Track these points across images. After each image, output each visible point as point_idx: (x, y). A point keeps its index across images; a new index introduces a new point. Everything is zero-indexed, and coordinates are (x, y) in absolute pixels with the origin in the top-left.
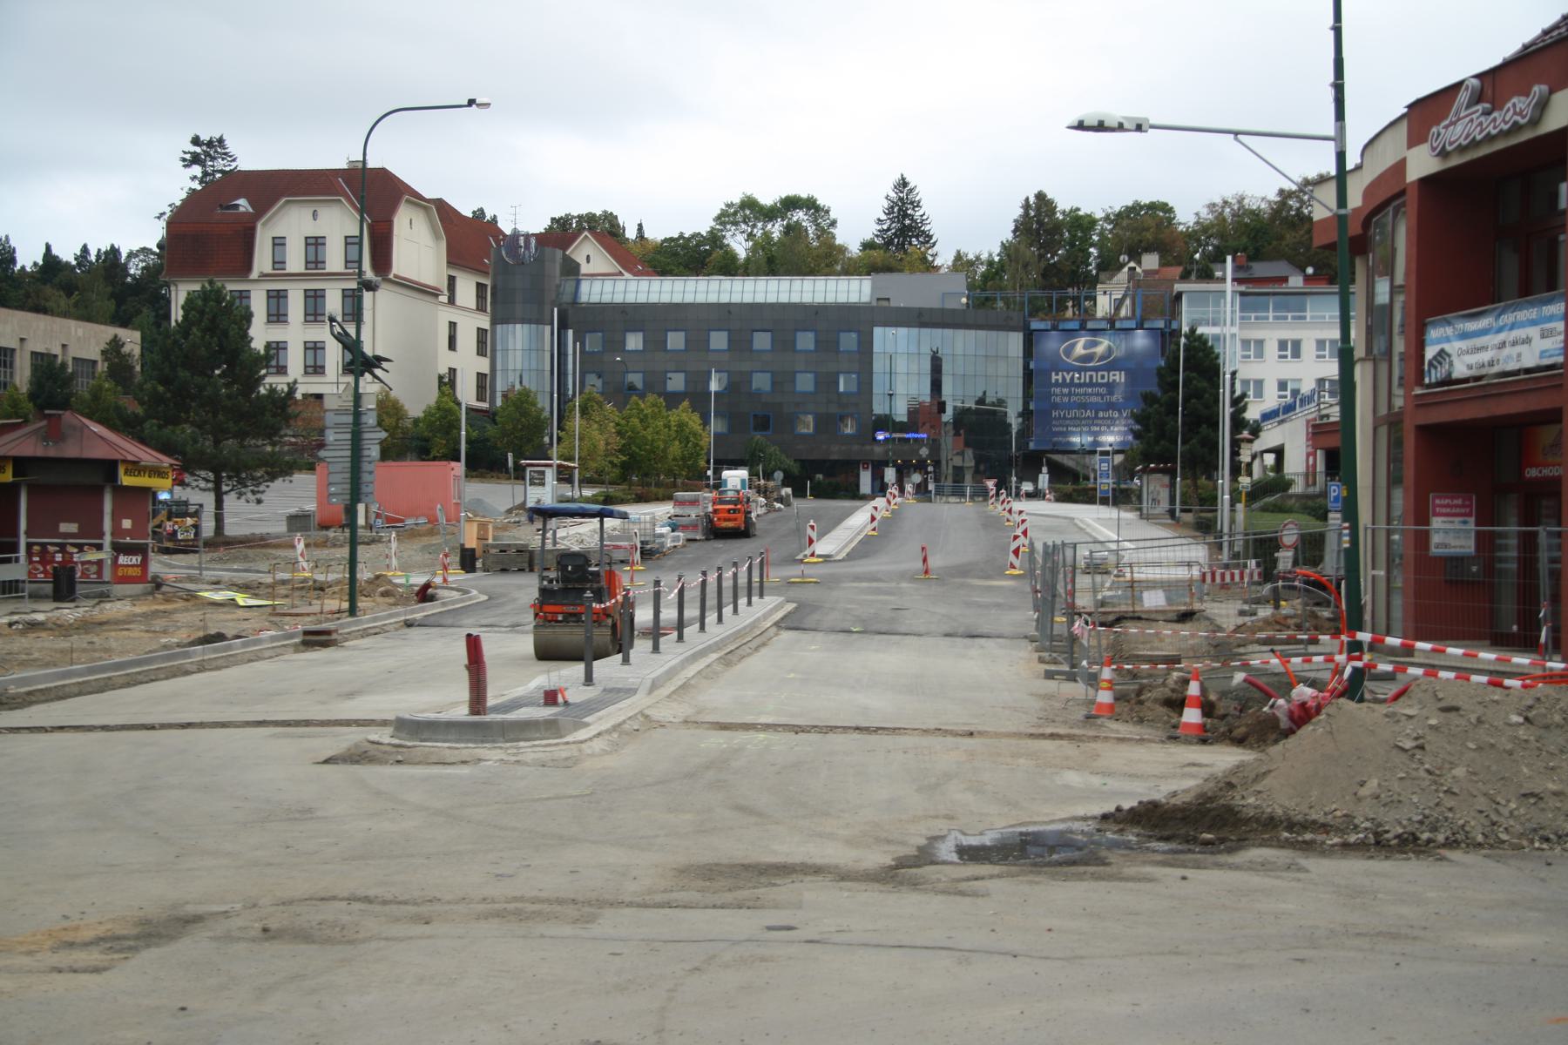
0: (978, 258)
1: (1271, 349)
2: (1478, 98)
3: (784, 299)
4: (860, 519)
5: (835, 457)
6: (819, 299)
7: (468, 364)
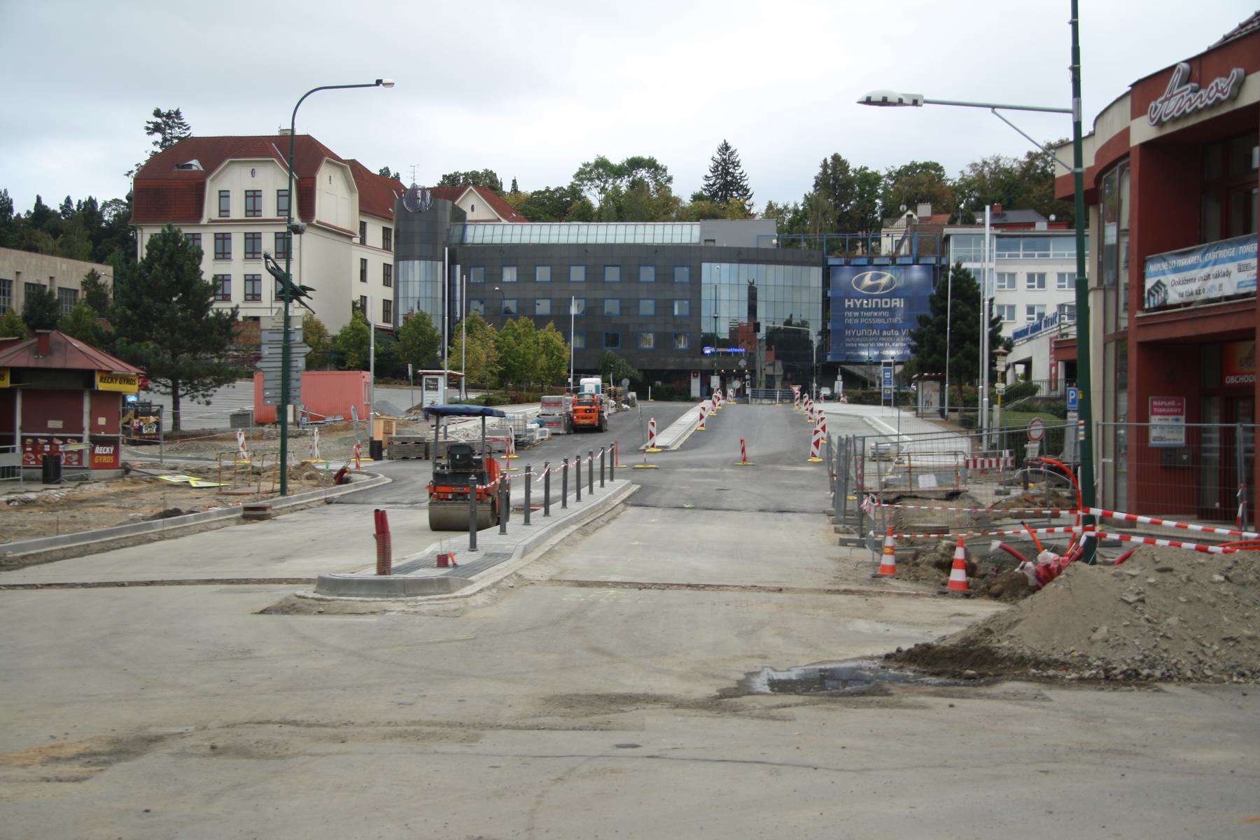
0: (786, 207)
1: (1022, 281)
2: (1188, 78)
3: (630, 240)
4: (691, 417)
5: (671, 367)
6: (658, 240)
7: (376, 293)
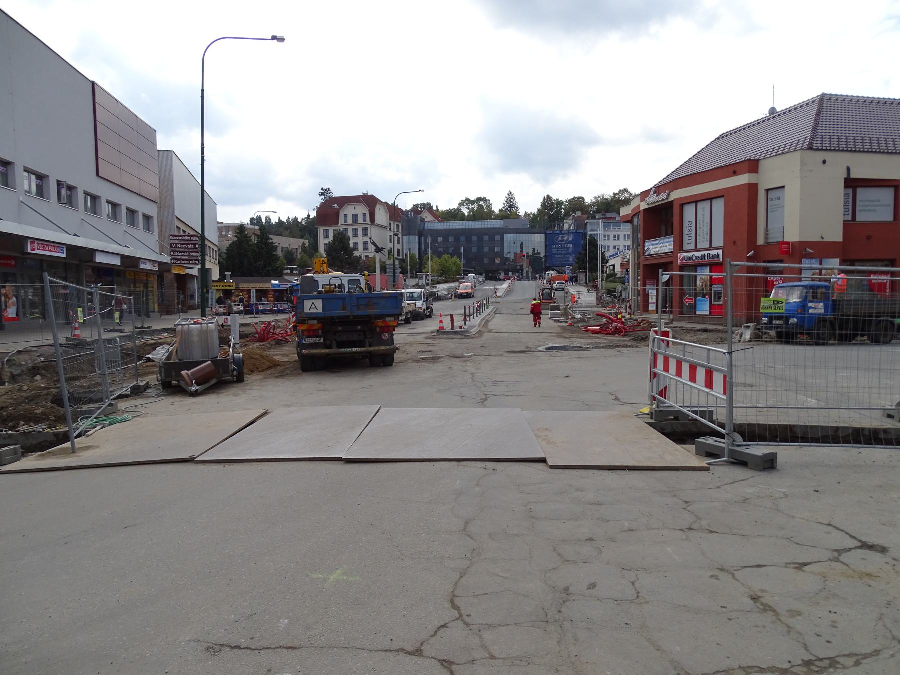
0: (531, 213)
1: (612, 237)
2: (655, 193)
4: (505, 285)
5: (494, 269)
6: (490, 226)
